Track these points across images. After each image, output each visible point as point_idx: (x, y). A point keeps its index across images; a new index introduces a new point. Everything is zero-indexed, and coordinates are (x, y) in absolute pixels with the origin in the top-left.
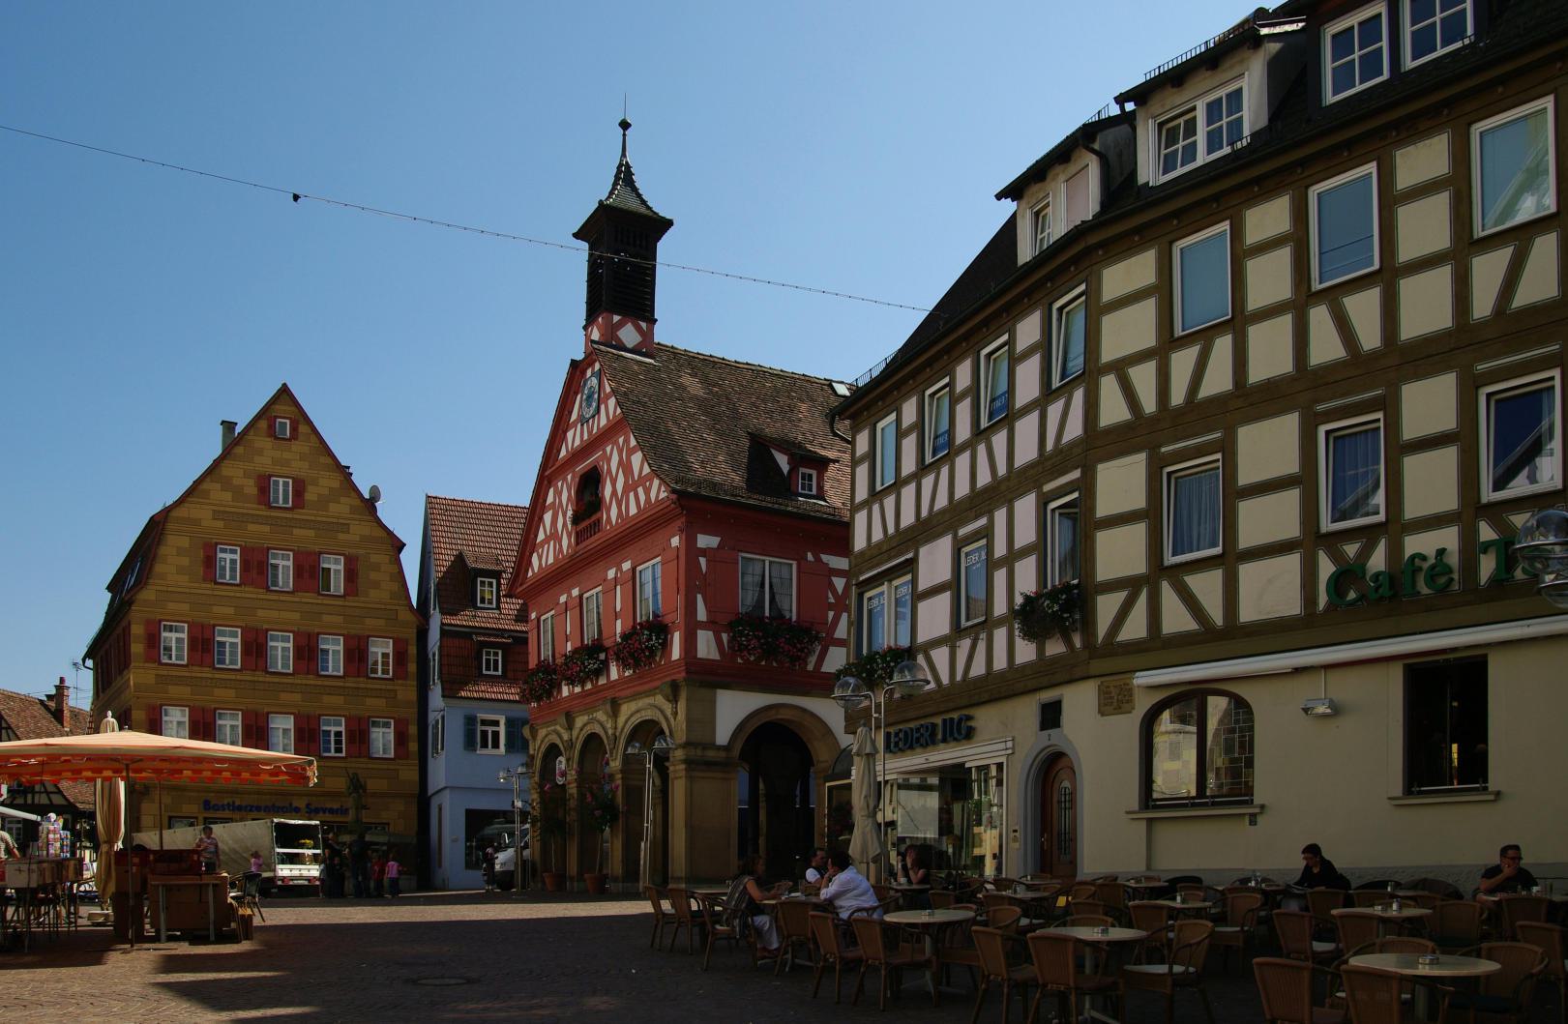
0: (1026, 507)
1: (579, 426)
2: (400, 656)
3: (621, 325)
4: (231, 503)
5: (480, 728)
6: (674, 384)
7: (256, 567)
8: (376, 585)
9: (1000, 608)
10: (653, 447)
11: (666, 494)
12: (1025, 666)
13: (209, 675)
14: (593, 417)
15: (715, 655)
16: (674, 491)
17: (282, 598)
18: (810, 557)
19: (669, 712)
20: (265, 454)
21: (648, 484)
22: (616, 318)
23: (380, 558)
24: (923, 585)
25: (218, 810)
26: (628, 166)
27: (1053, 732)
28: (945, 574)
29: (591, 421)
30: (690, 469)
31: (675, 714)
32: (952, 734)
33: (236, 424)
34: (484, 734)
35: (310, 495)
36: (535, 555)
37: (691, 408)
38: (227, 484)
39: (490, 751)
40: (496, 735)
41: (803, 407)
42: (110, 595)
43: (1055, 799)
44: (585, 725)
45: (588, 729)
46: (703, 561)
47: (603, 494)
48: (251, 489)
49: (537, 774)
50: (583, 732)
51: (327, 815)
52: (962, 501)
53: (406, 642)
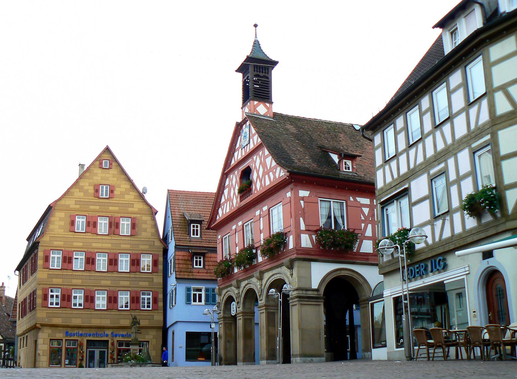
0: (464, 156)
1: (240, 149)
2: (155, 263)
3: (258, 105)
4: (83, 197)
5: (193, 293)
6: (283, 128)
7: (92, 224)
8: (145, 230)
9: (456, 203)
11: (284, 173)
12: (471, 230)
13: (71, 274)
14: (247, 145)
15: (310, 245)
16: (288, 172)
17: (103, 238)
18: (351, 199)
19: (288, 274)
20: (99, 176)
21: (274, 170)
22: (256, 103)
23: (147, 218)
24: (414, 199)
27: (490, 260)
28: (425, 192)
29: (246, 147)
30: (293, 162)
31: (292, 275)
32: (436, 268)
33: (84, 165)
34: (195, 295)
35: (117, 192)
36: (220, 209)
37: (291, 137)
38: (81, 189)
39: (197, 303)
40: (200, 296)
41: (342, 135)
42: (28, 242)
43: (494, 294)
44: (246, 285)
45: (248, 287)
46: (302, 202)
47: (253, 178)
48: (91, 190)
49: (222, 312)
50: (245, 288)
52: (430, 158)
53: (158, 255)
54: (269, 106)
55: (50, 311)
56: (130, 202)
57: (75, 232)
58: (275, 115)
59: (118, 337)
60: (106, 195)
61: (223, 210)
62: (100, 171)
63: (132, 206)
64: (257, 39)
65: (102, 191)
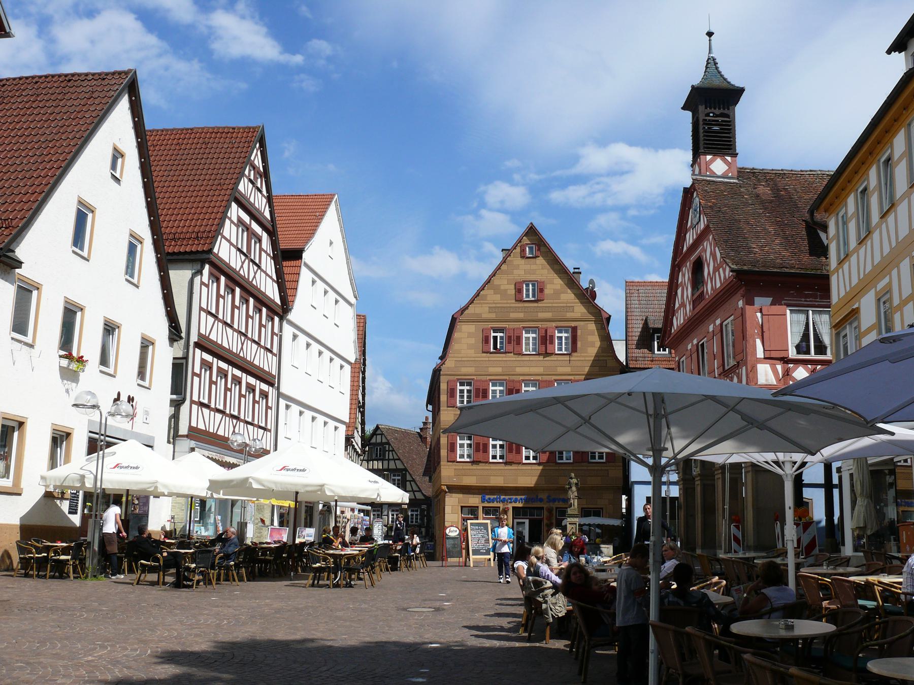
3: (712, 161)
10: (726, 241)
14: (698, 223)
17: (531, 359)
22: (709, 157)
25: (534, 502)
26: (714, 59)
36: (675, 317)
38: (497, 290)
48: (512, 291)
51: (561, 503)
54: (730, 161)
55: (460, 466)
56: (568, 305)
57: (491, 353)
58: (742, 173)
59: (557, 503)
60: (534, 296)
61: (677, 319)
62: (523, 261)
63: (572, 309)
64: (711, 55)
65: (528, 290)
